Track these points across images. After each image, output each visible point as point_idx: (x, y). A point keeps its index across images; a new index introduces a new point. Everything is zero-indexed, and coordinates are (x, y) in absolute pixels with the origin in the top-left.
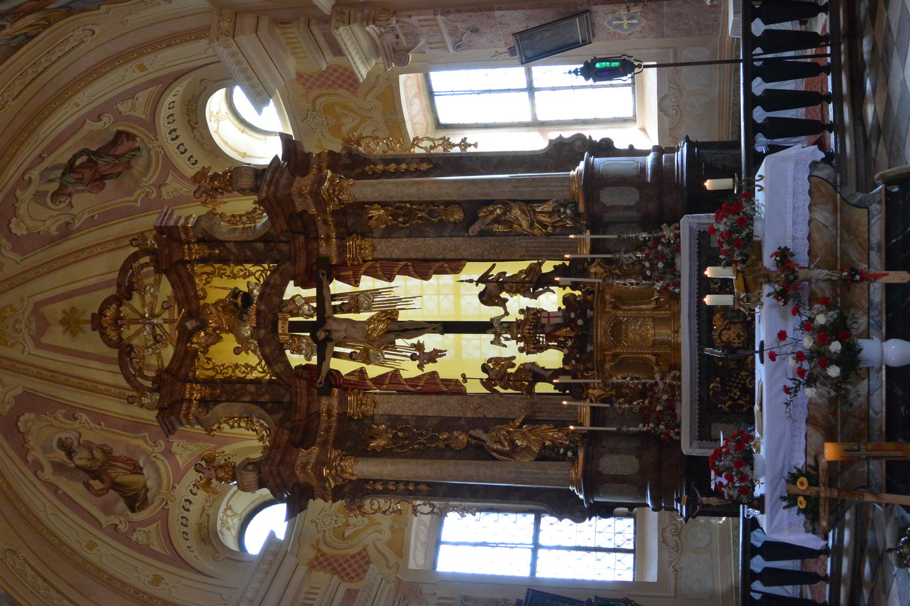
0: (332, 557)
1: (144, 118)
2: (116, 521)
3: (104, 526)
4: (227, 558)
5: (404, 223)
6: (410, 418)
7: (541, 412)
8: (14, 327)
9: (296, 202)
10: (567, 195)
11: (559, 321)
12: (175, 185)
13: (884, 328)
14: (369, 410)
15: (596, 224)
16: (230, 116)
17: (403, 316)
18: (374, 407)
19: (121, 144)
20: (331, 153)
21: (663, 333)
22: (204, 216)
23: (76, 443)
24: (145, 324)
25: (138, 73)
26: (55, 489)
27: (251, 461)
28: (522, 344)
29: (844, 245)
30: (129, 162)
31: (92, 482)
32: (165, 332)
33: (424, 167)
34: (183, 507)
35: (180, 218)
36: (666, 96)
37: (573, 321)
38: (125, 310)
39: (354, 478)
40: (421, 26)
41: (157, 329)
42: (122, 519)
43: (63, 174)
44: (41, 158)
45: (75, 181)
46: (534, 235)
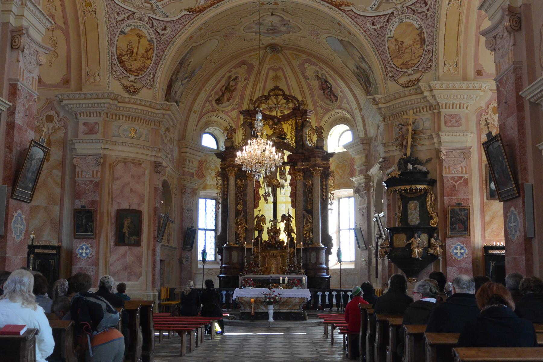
2: (213, 96)
10: (314, 242)
11: (277, 240)
15: (305, 250)
17: (278, 190)
20: (329, 167)
21: (273, 270)
25: (355, 108)
28: (270, 228)
31: (225, 87)
36: (345, 271)
37: (277, 244)
38: (281, 97)
39: (229, 176)
44: (329, 74)
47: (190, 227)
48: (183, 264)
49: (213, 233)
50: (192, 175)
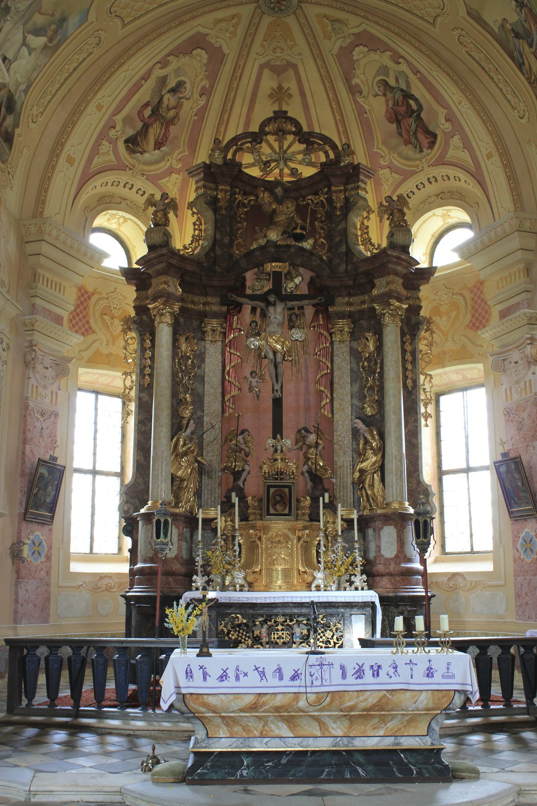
0: (88, 305)
1: (447, 157)
2: (118, 128)
3: (114, 118)
4: (87, 219)
5: (363, 367)
6: (203, 370)
7: (208, 478)
8: (278, 47)
9: (382, 279)
12: (391, 180)
13: (334, 749)
14: (209, 338)
16: (446, 226)
18: (211, 341)
19: (426, 137)
20: (420, 307)
22: (367, 203)
23: (181, 95)
24: (279, 154)
25: (485, 153)
26: (145, 78)
27: (169, 239)
29: (399, 716)
30: (411, 143)
32: (272, 170)
33: (409, 382)
34: (127, 183)
35: (366, 184)
38: (290, 138)
40: (525, 382)
41: (275, 163)
42: (119, 133)
43: (402, 90)
44: (416, 72)
45: (396, 100)
46: (353, 473)
47: (47, 458)
48: (23, 560)
49: (116, 482)
50: (58, 320)
